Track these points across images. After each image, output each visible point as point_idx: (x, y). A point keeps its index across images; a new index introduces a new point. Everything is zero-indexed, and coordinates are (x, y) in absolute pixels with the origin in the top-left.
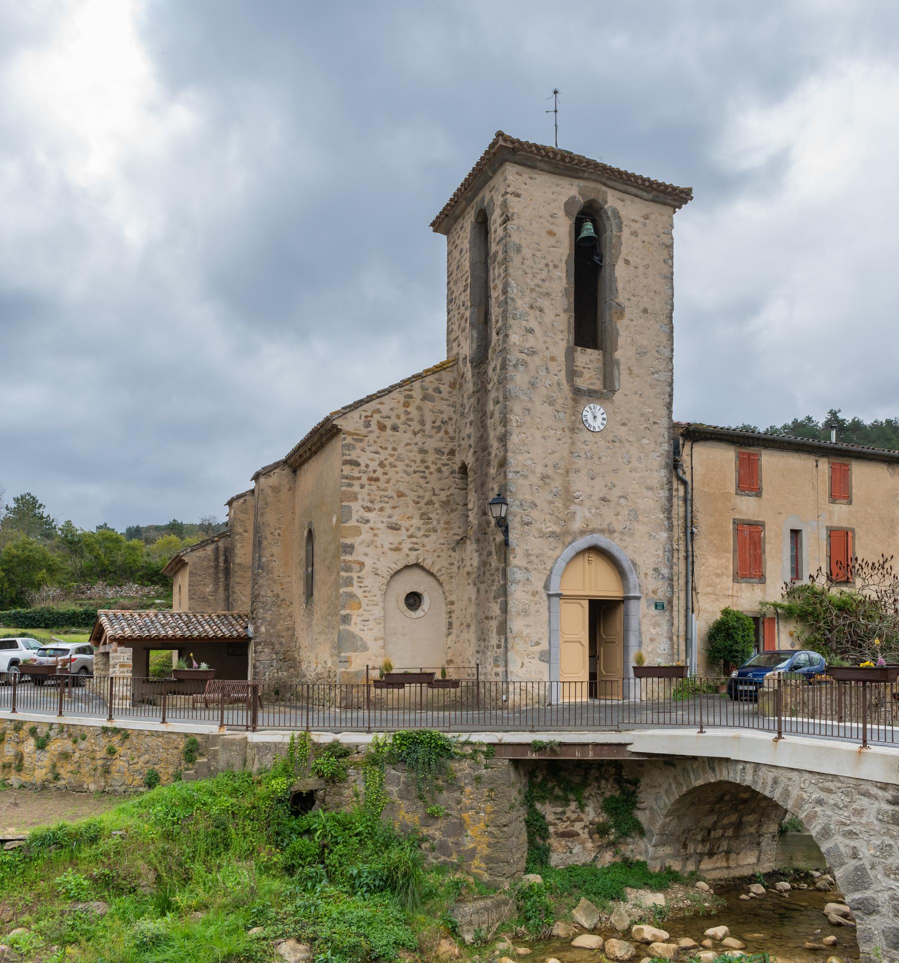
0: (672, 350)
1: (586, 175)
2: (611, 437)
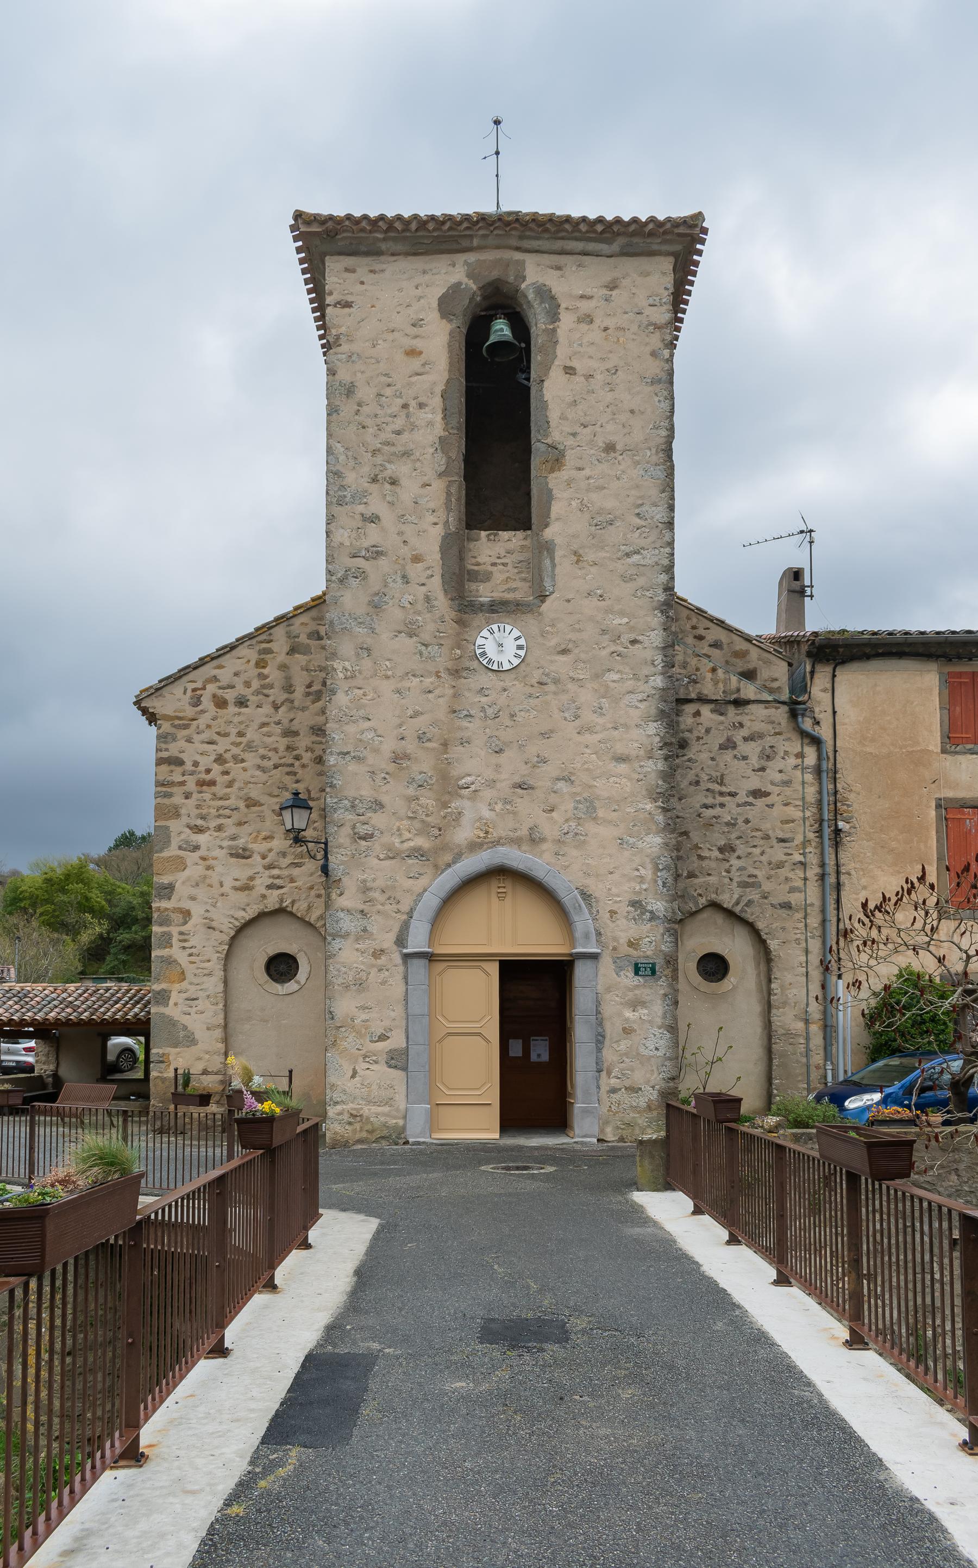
0: (671, 508)
1: (476, 242)
2: (537, 675)
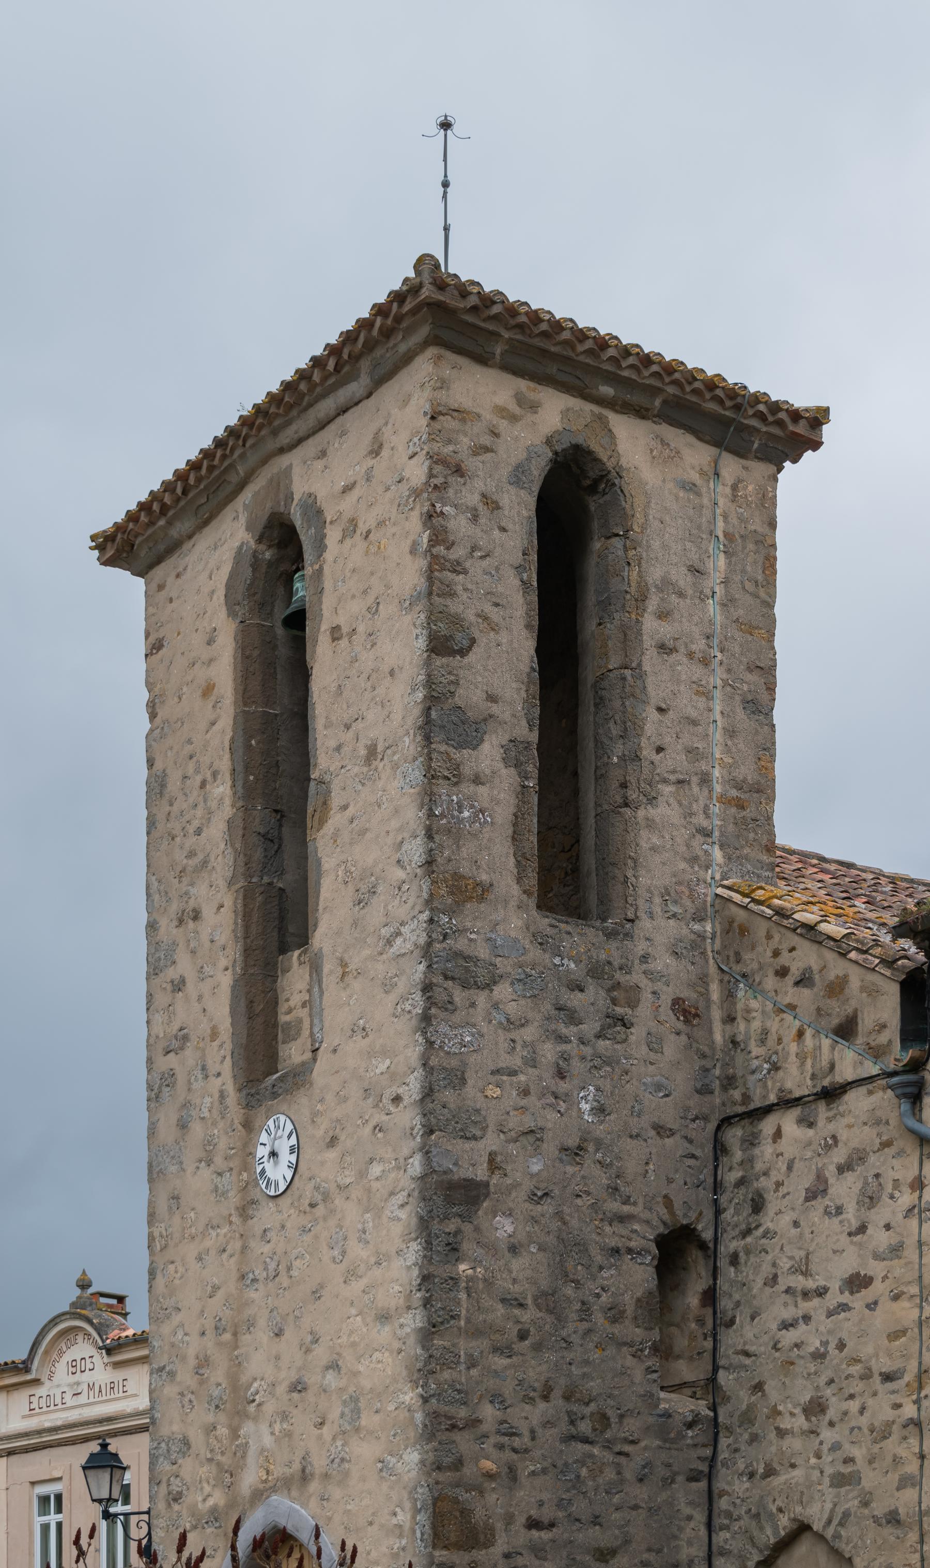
1: (241, 470)
